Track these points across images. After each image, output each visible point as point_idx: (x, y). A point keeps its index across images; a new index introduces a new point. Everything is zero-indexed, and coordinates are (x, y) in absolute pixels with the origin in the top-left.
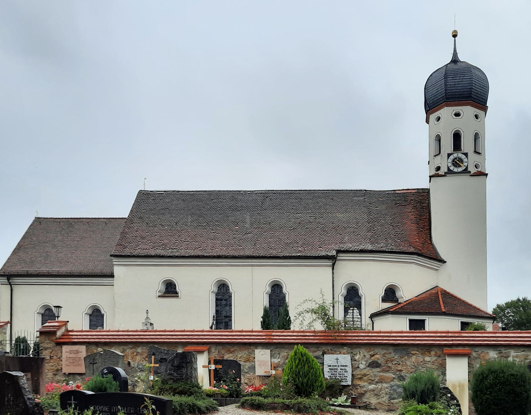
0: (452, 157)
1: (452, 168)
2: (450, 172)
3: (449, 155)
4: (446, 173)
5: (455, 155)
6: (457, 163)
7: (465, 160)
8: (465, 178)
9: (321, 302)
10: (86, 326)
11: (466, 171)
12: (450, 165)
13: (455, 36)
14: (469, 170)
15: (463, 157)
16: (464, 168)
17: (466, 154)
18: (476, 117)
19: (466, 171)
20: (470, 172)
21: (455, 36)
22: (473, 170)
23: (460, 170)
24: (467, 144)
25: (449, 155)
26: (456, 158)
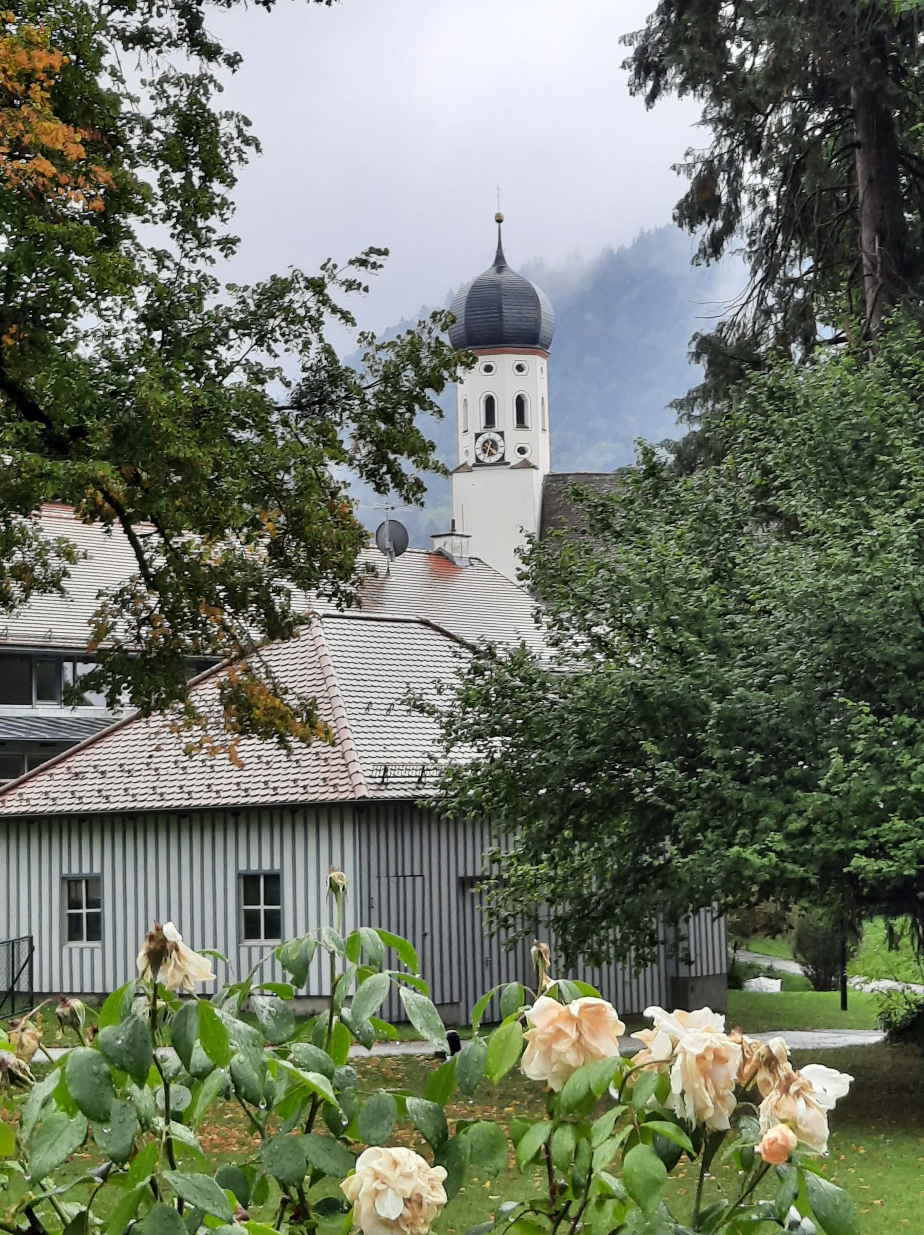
0: (481, 439)
1: (481, 458)
2: (479, 463)
3: (478, 436)
4: (474, 466)
5: (486, 436)
6: (490, 446)
7: (500, 443)
8: (501, 473)
9: (517, 644)
10: (313, 1203)
11: (502, 462)
12: (479, 451)
13: (499, 221)
14: (507, 460)
15: (497, 438)
16: (499, 456)
17: (501, 434)
18: (520, 368)
19: (502, 462)
20: (508, 463)
21: (499, 221)
22: (513, 458)
23: (494, 459)
24: (506, 414)
25: (478, 436)
26: (487, 441)
